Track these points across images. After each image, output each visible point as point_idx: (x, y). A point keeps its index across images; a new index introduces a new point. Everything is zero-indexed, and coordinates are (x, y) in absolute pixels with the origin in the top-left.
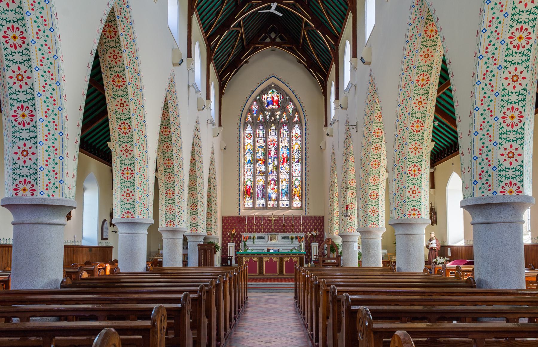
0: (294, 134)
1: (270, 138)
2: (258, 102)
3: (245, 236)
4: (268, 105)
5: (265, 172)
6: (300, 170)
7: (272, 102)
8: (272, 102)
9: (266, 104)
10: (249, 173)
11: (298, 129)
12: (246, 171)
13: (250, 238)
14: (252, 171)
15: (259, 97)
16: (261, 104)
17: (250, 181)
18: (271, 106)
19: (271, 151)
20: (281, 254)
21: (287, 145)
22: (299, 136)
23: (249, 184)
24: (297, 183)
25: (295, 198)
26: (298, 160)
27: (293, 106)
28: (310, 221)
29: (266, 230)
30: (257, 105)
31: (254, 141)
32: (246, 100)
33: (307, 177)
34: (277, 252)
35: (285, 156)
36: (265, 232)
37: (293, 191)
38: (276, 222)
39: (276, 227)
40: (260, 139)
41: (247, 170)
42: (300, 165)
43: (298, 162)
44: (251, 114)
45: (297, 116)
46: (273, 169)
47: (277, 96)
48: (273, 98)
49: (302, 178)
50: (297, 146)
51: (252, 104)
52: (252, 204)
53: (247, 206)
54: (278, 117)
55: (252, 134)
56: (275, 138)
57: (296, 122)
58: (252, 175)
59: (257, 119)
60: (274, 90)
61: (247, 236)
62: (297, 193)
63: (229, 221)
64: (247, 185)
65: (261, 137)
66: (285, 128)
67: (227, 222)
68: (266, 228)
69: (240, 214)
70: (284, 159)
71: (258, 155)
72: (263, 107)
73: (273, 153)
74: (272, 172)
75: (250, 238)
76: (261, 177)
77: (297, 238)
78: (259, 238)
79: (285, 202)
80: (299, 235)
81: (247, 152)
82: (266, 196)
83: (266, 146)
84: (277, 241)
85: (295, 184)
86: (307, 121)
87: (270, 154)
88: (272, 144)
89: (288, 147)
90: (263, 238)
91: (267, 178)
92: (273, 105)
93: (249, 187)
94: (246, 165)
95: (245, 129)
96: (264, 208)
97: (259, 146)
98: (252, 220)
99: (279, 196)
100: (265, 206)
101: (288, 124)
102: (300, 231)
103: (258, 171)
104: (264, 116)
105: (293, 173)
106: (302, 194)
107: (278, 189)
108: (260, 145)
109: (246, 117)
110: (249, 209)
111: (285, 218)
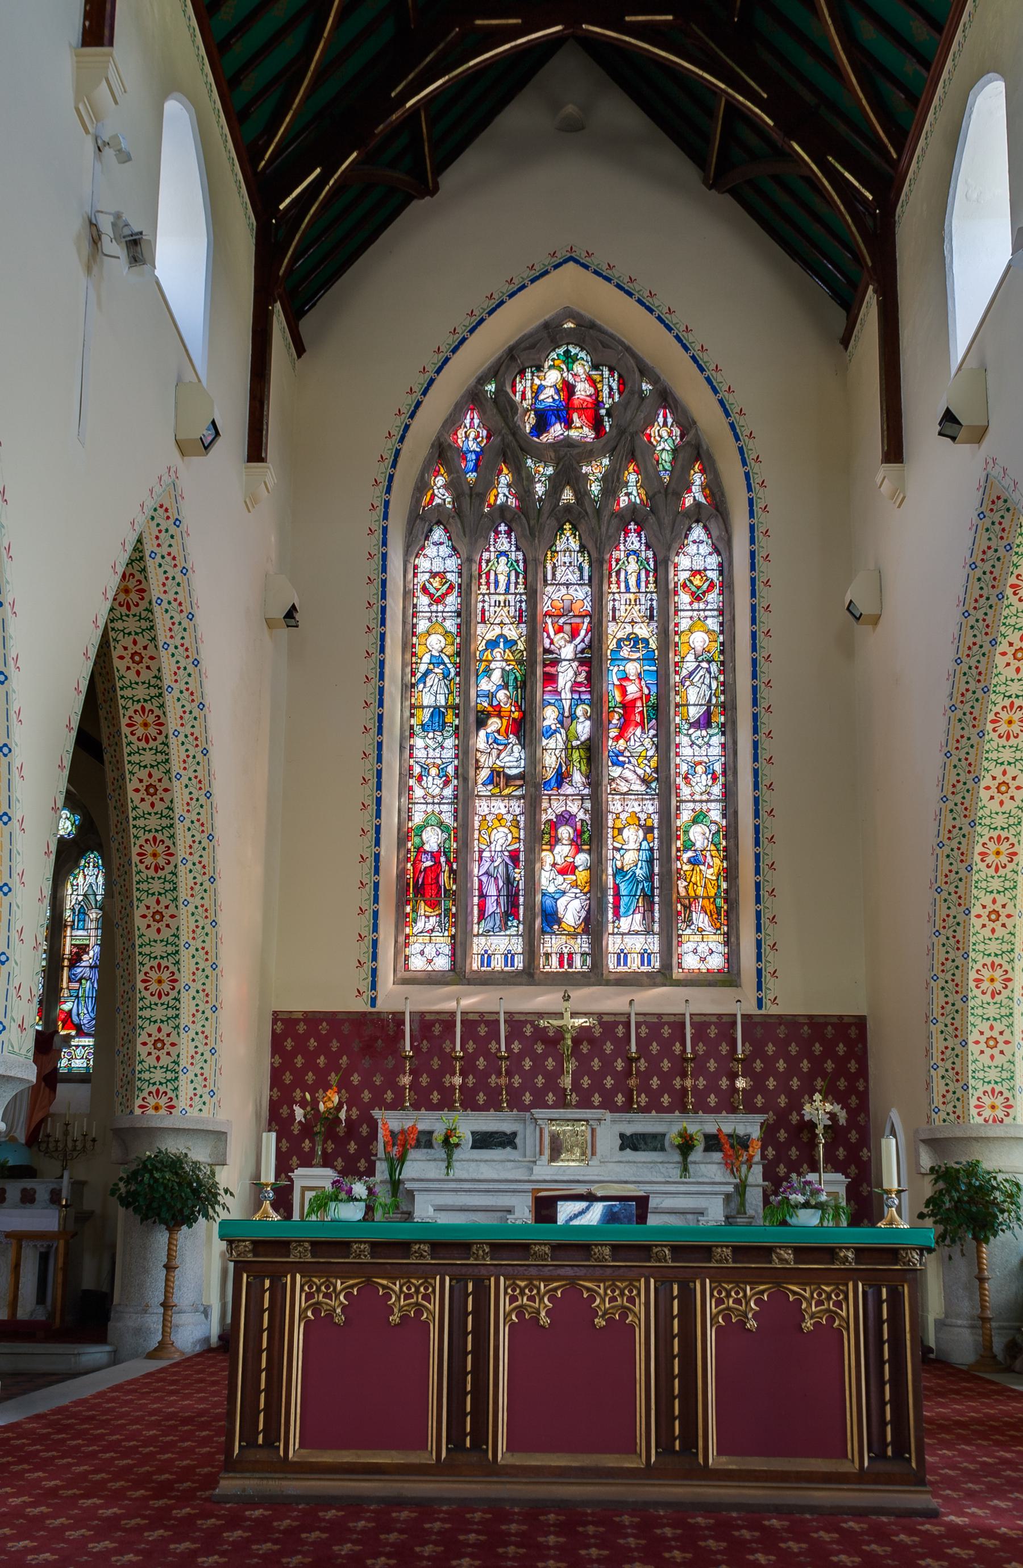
0: (684, 576)
1: (552, 597)
2: (489, 406)
3: (395, 1125)
4: (542, 425)
5: (521, 776)
6: (718, 768)
7: (563, 413)
8: (563, 413)
9: (531, 419)
10: (433, 783)
11: (705, 549)
12: (417, 770)
13: (425, 1140)
14: (450, 770)
15: (491, 387)
16: (505, 419)
17: (441, 824)
18: (557, 430)
19: (555, 662)
20: (679, 1251)
21: (643, 631)
22: (712, 586)
23: (432, 839)
24: (698, 835)
25: (689, 922)
26: (708, 714)
27: (677, 431)
28: (782, 1045)
29: (527, 1098)
30: (483, 424)
31: (465, 615)
32: (424, 379)
33: (765, 794)
34: (629, 1233)
35: (632, 689)
36: (516, 1103)
37: (682, 884)
38: (585, 1048)
39: (586, 1082)
40: (497, 604)
41: (425, 768)
42: (717, 740)
43: (708, 725)
44: (449, 472)
45: (697, 479)
46: (569, 761)
47: (592, 382)
48: (568, 389)
49: (730, 810)
50: (699, 640)
51: (453, 422)
52: (447, 950)
53: (417, 963)
54: (595, 488)
55: (452, 577)
56: (581, 595)
57: (697, 514)
58: (448, 792)
59: (482, 497)
60: (574, 351)
61: (408, 1125)
62: (700, 891)
63: (313, 1043)
64: (420, 850)
65: (502, 589)
66: (634, 542)
67: (301, 1046)
68: (528, 1085)
69: (373, 1001)
70: (628, 707)
71: (485, 685)
72: (515, 431)
73: (566, 675)
74: (562, 777)
75: (425, 1140)
76: (499, 807)
77: (713, 1143)
78: (483, 1141)
79: (637, 943)
80: (730, 1124)
81: (423, 668)
82: (530, 907)
83: (532, 639)
84: (594, 1162)
85: (689, 845)
86: (759, 492)
87: (551, 679)
88: (560, 630)
89: (653, 645)
90: (506, 1141)
91: (533, 807)
92: (568, 424)
93: (435, 856)
94: (419, 742)
95: (414, 546)
96: (518, 974)
97: (490, 636)
98: (442, 1037)
99: (602, 910)
100: (519, 964)
101: (652, 519)
102: (728, 1105)
103: (484, 774)
104: (523, 483)
105: (679, 780)
106: (731, 898)
107: (596, 869)
108: (497, 631)
109: (422, 486)
110: (432, 979)
111: (638, 1025)
